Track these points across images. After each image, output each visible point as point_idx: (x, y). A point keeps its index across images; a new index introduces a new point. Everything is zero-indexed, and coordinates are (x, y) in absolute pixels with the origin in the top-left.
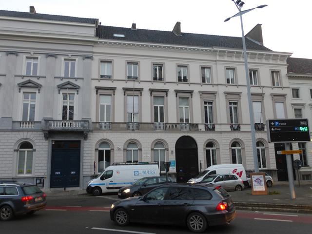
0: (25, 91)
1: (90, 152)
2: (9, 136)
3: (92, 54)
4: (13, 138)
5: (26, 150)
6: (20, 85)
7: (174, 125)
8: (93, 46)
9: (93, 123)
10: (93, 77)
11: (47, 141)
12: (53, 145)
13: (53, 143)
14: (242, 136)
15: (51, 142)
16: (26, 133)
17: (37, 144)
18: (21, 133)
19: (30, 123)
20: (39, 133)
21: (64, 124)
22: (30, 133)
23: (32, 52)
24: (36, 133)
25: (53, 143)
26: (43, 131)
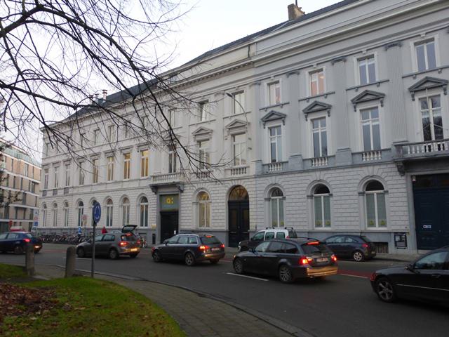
0: (270, 126)
4: (355, 177)
5: (375, 192)
11: (403, 178)
13: (414, 180)
14: (381, 171)
15: (409, 178)
18: (365, 169)
20: (389, 166)
22: (376, 168)
23: (271, 75)
24: (385, 166)
25: (414, 180)
26: (395, 162)
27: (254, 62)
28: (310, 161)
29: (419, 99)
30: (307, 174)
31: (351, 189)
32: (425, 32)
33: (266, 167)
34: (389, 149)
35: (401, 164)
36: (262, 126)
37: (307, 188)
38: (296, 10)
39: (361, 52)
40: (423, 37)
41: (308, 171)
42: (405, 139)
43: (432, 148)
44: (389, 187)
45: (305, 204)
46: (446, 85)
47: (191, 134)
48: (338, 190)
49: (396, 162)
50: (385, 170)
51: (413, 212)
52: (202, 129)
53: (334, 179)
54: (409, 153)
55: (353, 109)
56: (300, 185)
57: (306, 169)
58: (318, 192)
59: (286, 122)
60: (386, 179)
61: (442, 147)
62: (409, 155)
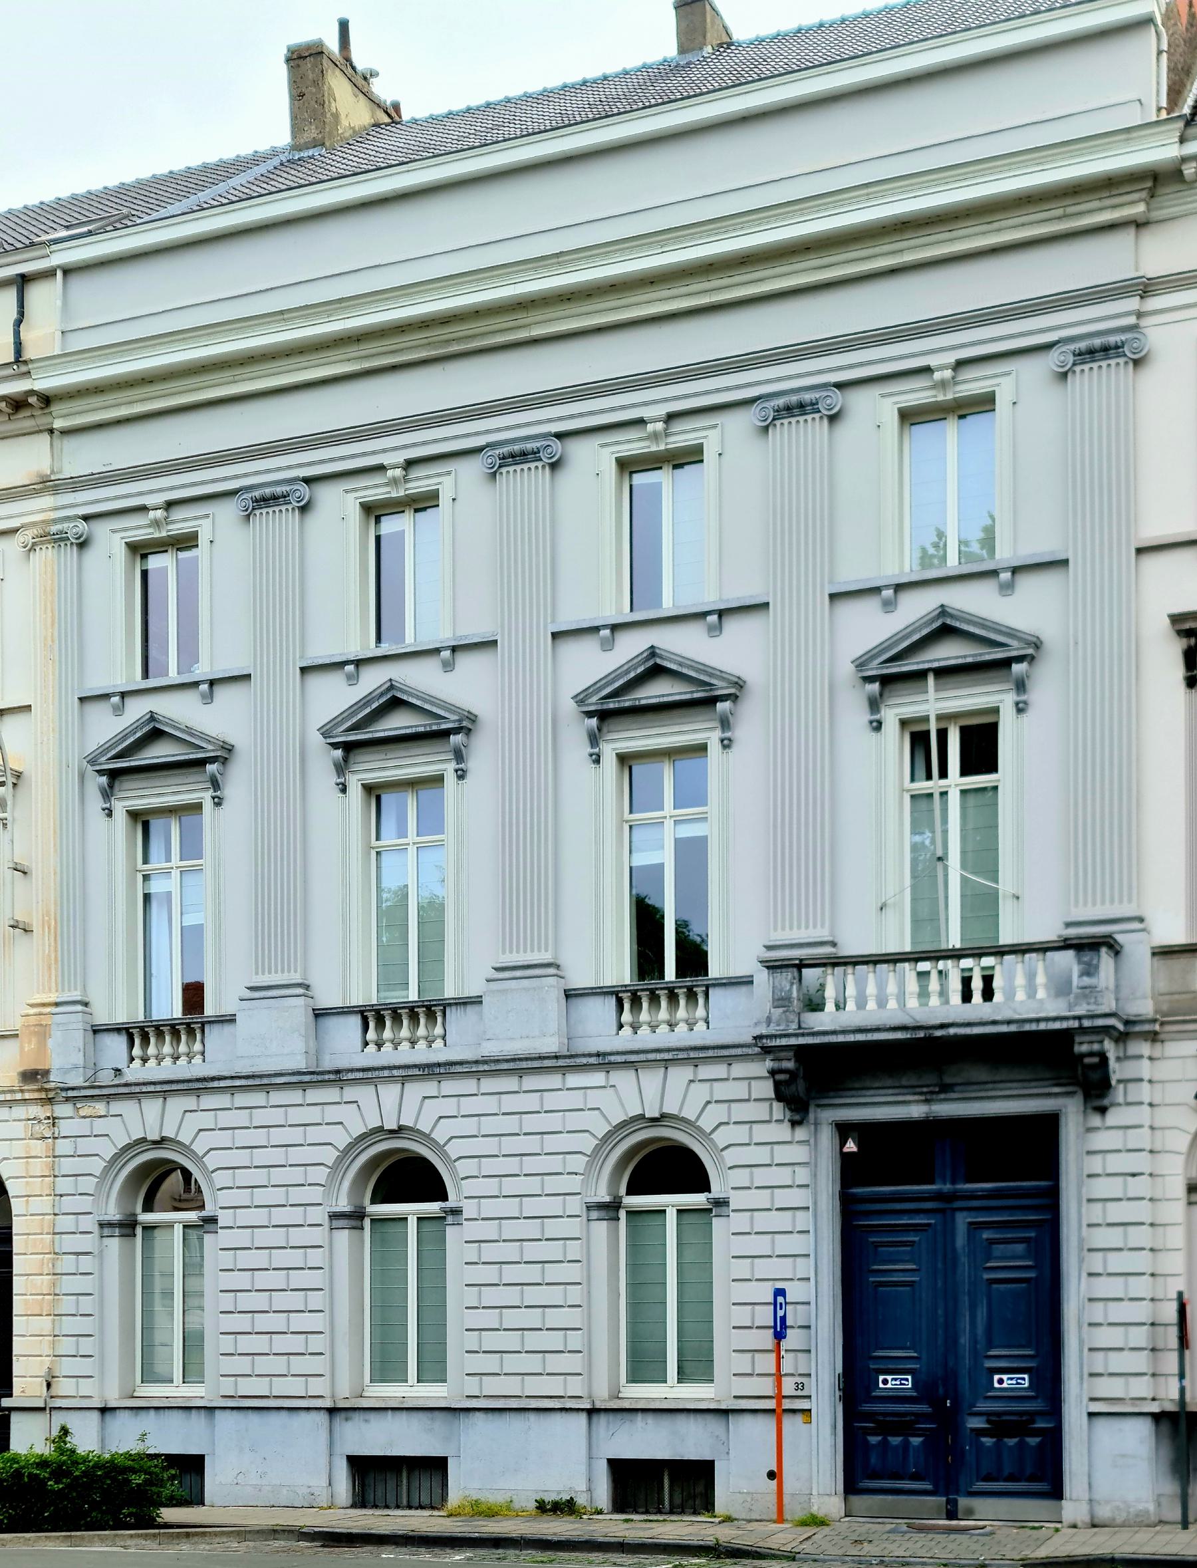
0: (139, 804)
1: (1140, 1212)
2: (551, 1101)
3: (1133, 303)
4: (314, 1134)
5: (671, 1202)
6: (593, 703)
7: (626, 997)
8: (1139, 224)
9: (1165, 953)
10: (1154, 530)
11: (801, 1133)
12: (845, 1158)
13: (851, 1146)
14: (700, 1093)
15: (827, 1137)
16: (395, 1089)
17: (731, 1156)
18: (623, 1079)
19: (645, 996)
20: (739, 1069)
21: (977, 985)
22: (680, 1075)
23: (154, 491)
24: (719, 1070)
25: (851, 1146)
26: (764, 1047)
27: (47, 400)
28: (356, 1021)
29: (904, 723)
30: (331, 1094)
31: (552, 1184)
32: (951, 358)
33: (117, 1044)
34: (747, 981)
35: (790, 1065)
36: (96, 803)
37: (334, 1168)
38: (338, 86)
39: (927, 370)
40: (943, 385)
41: (338, 1077)
42: (822, 934)
43: (997, 983)
44: (226, 1198)
45: (315, 1257)
46: (734, 698)
47: (316, 739)
48: (491, 1186)
49: (767, 1050)
50: (721, 1091)
51: (120, 1317)
52: (155, 734)
53: (469, 1126)
54: (1041, 979)
55: (866, 716)
56: (296, 1155)
57: (328, 1064)
58: (384, 1194)
59: (474, 764)
60: (721, 1138)
61: (977, 985)
62: (825, 1021)
